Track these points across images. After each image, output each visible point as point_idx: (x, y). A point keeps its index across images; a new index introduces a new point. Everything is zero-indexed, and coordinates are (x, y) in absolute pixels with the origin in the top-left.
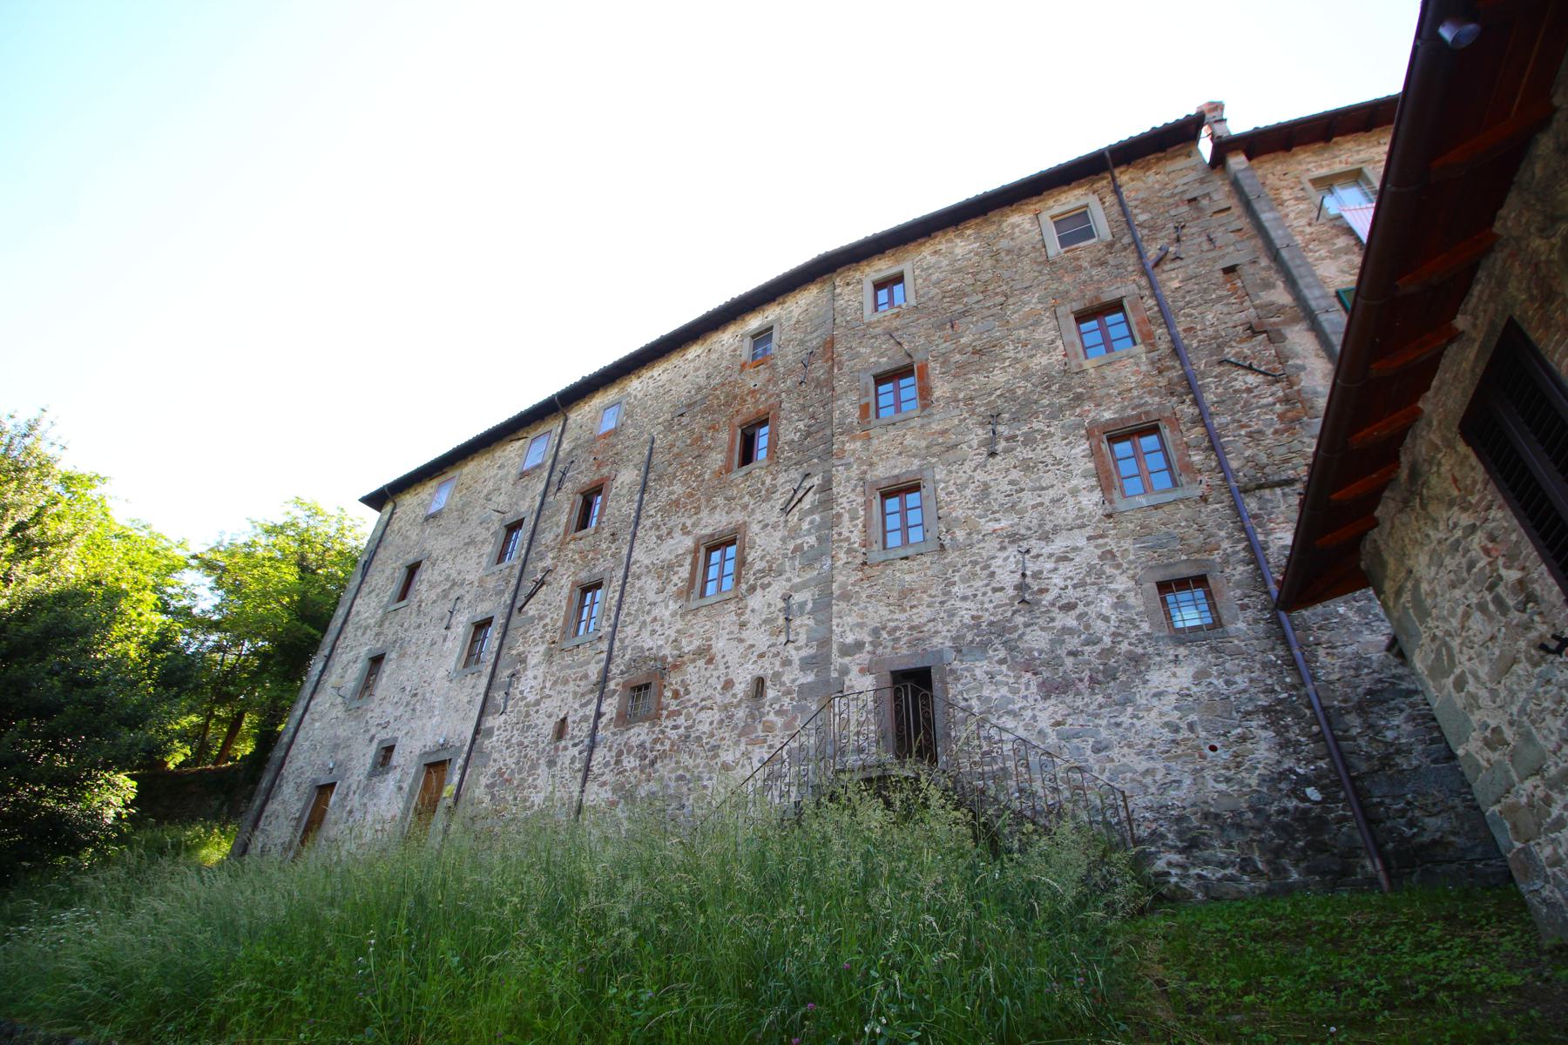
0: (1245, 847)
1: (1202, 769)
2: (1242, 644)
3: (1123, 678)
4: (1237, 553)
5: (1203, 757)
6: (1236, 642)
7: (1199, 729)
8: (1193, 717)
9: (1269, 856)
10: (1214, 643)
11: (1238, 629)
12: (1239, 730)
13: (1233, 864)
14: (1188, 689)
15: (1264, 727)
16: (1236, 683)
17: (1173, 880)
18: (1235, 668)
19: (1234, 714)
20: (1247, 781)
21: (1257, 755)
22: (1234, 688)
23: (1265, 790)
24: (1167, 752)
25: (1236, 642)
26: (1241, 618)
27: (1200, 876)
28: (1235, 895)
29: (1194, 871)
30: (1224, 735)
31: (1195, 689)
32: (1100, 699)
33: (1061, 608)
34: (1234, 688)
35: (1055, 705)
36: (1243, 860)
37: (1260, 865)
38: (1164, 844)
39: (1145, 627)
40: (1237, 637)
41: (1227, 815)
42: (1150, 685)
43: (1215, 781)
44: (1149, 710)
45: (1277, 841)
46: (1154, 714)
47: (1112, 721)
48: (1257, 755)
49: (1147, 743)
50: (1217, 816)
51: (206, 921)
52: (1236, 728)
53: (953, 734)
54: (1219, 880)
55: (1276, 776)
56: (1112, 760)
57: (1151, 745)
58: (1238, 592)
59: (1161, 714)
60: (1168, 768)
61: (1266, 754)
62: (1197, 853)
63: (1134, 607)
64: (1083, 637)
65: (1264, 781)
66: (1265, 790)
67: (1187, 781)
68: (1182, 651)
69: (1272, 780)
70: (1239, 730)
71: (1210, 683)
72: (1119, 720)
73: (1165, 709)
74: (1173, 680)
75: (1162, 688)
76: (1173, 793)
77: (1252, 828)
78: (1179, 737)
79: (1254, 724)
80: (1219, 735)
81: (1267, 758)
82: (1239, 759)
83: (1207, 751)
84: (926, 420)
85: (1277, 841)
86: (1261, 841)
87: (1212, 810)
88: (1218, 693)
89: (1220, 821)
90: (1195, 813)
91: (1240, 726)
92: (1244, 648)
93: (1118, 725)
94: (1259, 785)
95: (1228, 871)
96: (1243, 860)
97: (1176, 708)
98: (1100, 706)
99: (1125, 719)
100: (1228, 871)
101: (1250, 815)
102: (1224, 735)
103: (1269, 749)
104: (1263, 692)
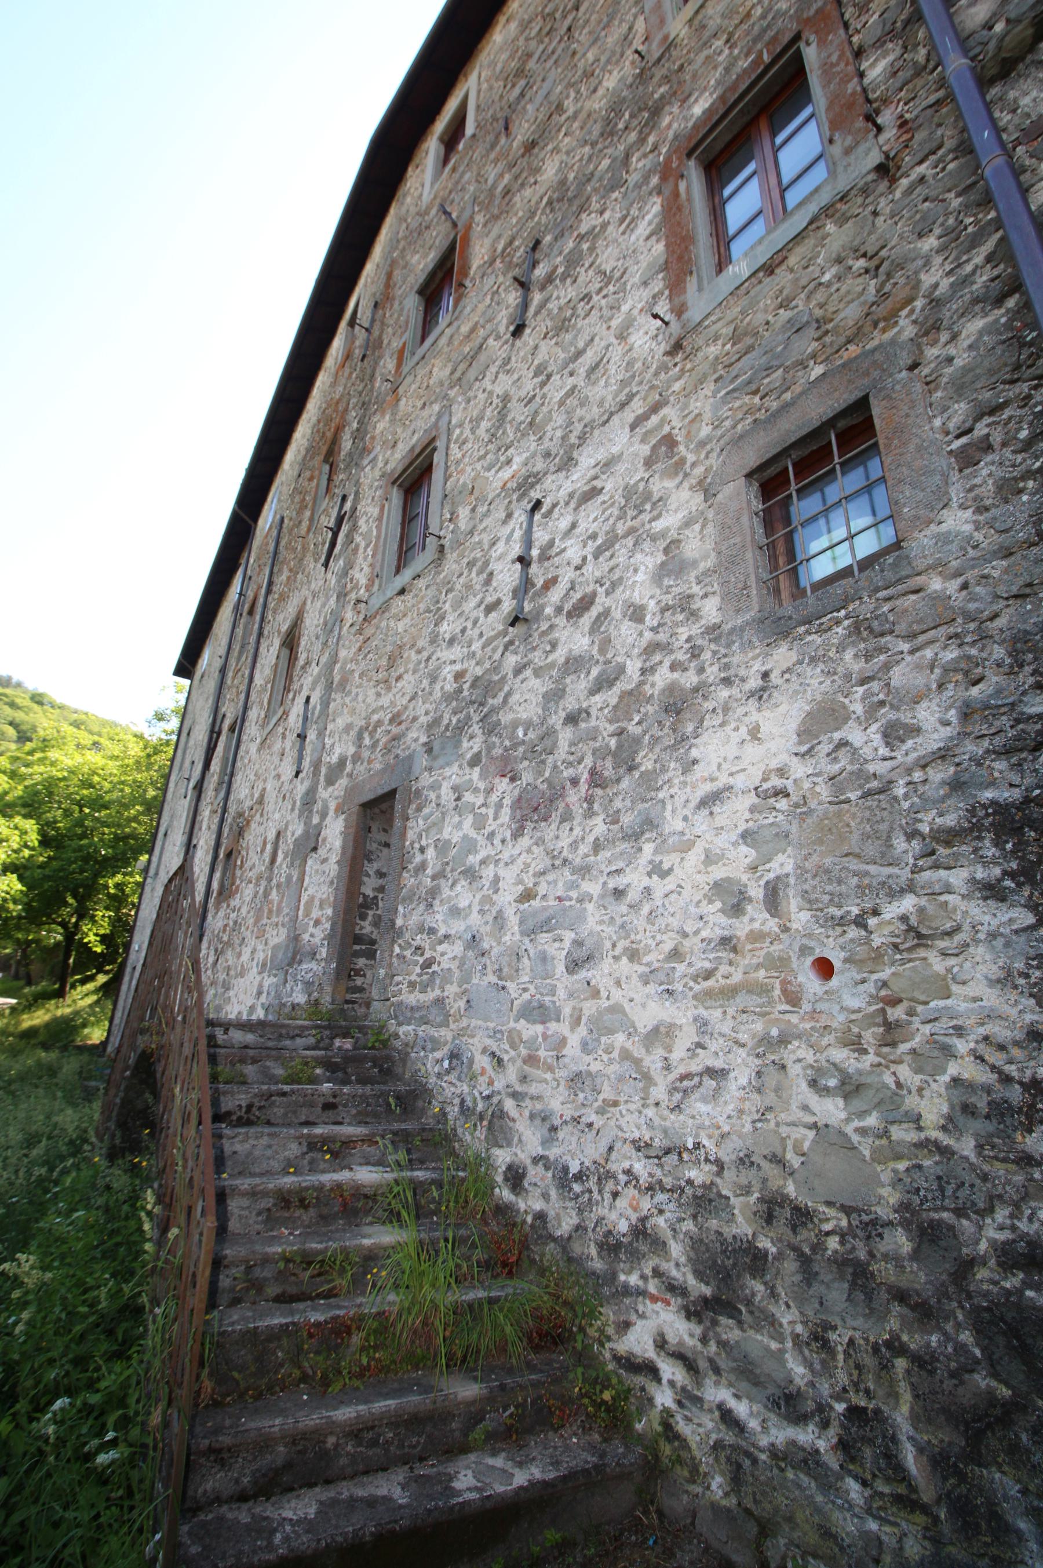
0: (869, 1361)
1: (783, 1040)
2: (954, 584)
3: (648, 765)
4: (966, 281)
5: (793, 999)
6: (936, 584)
7: (793, 903)
8: (783, 864)
9: (944, 1436)
10: (865, 607)
11: (944, 539)
12: (908, 904)
13: (822, 1416)
14: (781, 772)
15: (992, 892)
16: (916, 730)
17: (664, 1398)
18: (920, 680)
19: (900, 843)
20: (911, 1102)
21: (959, 1002)
22: (911, 750)
23: (967, 1147)
24: (708, 975)
25: (936, 584)
26: (956, 493)
27: (726, 1416)
28: (813, 1538)
29: (717, 1393)
30: (860, 922)
31: (799, 770)
32: (599, 826)
33: (570, 615)
34: (911, 750)
35: (529, 851)
36: (854, 1412)
37: (909, 1457)
38: (657, 1273)
39: (711, 610)
40: (939, 566)
41: (834, 1220)
42: (699, 771)
43: (813, 1083)
44: (686, 847)
45: (981, 1380)
46: (695, 857)
47: (611, 885)
48: (959, 1002)
49: (668, 947)
50: (802, 1216)
51: (751, 485)
52: (895, 894)
53: (399, 922)
54: (773, 1451)
55: (1015, 1095)
56: (596, 994)
57: (676, 954)
58: (960, 411)
59: (710, 859)
60: (702, 1025)
61: (992, 998)
62: (729, 1330)
63: (695, 563)
64: (595, 672)
65: (968, 1110)
66: (967, 1147)
67: (741, 1077)
68: (783, 655)
69: (999, 1110)
70: (908, 904)
71: (843, 744)
72: (620, 882)
73: (721, 842)
74: (752, 751)
75: (723, 780)
76: (703, 1108)
77: (901, 1296)
78: (741, 928)
79: (957, 878)
80: (841, 922)
81: (990, 1016)
82: (896, 1013)
83: (810, 982)
84: (599, 43)
85: (981, 1380)
86: (923, 1362)
87: (791, 1189)
88: (861, 775)
89: (805, 1237)
90: (747, 1191)
91: (910, 888)
92: (959, 599)
93: (619, 893)
94: (949, 1125)
95: (806, 1436)
96: (854, 1412)
97: (746, 836)
98: (597, 847)
99: (635, 879)
100: (806, 1436)
101: (900, 1242)
102: (860, 922)
103: (1005, 980)
104: (1006, 752)
